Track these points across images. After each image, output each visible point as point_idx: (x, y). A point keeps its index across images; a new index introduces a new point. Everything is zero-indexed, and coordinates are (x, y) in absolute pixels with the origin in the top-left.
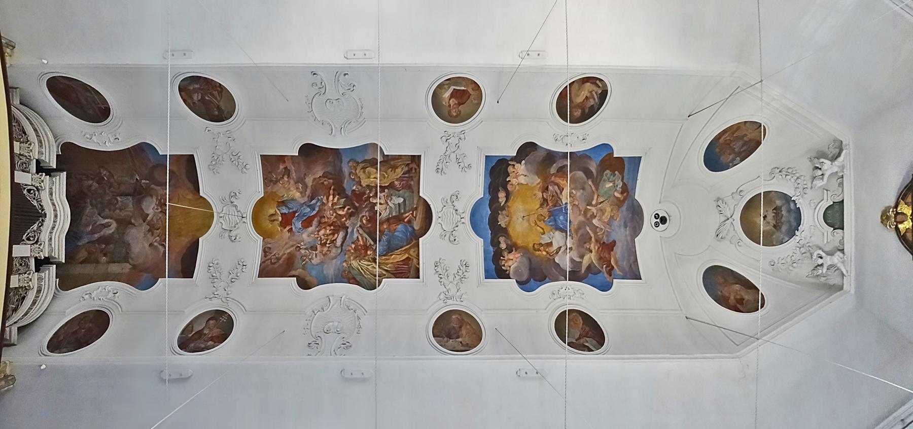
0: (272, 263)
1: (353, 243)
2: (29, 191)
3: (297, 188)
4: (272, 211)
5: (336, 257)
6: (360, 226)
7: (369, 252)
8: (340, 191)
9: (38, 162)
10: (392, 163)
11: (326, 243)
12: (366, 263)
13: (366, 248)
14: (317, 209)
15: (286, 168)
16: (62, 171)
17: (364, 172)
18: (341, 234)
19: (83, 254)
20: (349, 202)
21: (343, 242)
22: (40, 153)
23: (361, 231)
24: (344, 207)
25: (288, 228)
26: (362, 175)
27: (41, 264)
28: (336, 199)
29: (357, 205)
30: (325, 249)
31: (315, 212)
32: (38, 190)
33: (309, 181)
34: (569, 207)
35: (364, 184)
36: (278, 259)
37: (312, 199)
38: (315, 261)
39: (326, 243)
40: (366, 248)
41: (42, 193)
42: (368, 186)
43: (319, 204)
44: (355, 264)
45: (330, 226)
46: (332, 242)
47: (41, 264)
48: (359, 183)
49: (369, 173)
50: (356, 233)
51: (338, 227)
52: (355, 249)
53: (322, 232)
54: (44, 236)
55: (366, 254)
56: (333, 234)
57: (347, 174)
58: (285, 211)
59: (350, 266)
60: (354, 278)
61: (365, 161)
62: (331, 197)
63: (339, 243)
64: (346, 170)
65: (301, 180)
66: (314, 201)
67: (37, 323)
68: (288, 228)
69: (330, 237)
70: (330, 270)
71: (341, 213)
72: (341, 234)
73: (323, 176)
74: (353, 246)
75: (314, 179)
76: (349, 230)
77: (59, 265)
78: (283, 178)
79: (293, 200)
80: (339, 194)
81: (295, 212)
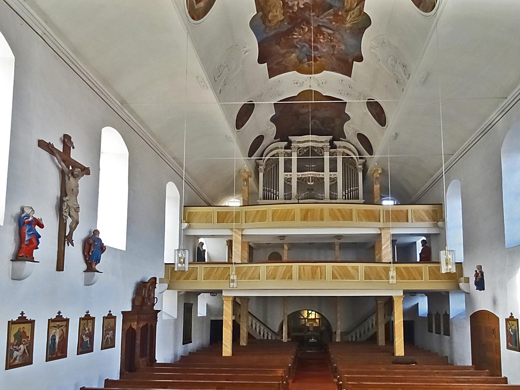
0: (342, 69)
1: (331, 23)
2: (300, 153)
3: (290, 56)
4: (306, 66)
5: (342, 36)
6: (318, 17)
7: (340, 13)
8: (290, 32)
9: (285, 149)
10: (262, 4)
11: (330, 39)
12: (349, 17)
13: (336, 15)
14: (304, 44)
15: (276, 65)
16: (288, 138)
17: (272, 20)
18: (324, 29)
19: (329, 130)
20: (298, 25)
21: (330, 29)
22: (281, 148)
23: (322, 16)
24: (302, 28)
25: (318, 58)
26: (274, 22)
27: (333, 146)
28: (296, 34)
29: (299, 20)
30: (335, 40)
31: (306, 45)
32: (299, 148)
33: (283, 51)
35: (283, 17)
36: (339, 65)
37: (297, 47)
38: (343, 47)
39: (330, 39)
40: (336, 15)
41: (300, 146)
42: (283, 15)
43: (300, 43)
44: (348, 25)
45: (317, 36)
46: (329, 35)
47: (333, 146)
48: (282, 21)
49: (273, 17)
50: (325, 18)
51: (318, 30)
52: (336, 22)
53: (321, 40)
54: (320, 145)
55: (342, 16)
56: (323, 34)
57: (276, 31)
58: (306, 60)
59: (350, 28)
60: (360, 29)
61: (264, 23)
62: (295, 37)
63: (330, 32)
64: (273, 33)
65: (284, 56)
66: (298, 46)
67: (359, 149)
68: (318, 58)
69: (326, 36)
70: (351, 41)
71: (307, 29)
72: (324, 29)
73: (279, 45)
74: (334, 23)
75: (282, 49)
76: (321, 24)
77: (334, 139)
78: (281, 40)
79: (297, 57)
80: (292, 32)
81: (307, 55)
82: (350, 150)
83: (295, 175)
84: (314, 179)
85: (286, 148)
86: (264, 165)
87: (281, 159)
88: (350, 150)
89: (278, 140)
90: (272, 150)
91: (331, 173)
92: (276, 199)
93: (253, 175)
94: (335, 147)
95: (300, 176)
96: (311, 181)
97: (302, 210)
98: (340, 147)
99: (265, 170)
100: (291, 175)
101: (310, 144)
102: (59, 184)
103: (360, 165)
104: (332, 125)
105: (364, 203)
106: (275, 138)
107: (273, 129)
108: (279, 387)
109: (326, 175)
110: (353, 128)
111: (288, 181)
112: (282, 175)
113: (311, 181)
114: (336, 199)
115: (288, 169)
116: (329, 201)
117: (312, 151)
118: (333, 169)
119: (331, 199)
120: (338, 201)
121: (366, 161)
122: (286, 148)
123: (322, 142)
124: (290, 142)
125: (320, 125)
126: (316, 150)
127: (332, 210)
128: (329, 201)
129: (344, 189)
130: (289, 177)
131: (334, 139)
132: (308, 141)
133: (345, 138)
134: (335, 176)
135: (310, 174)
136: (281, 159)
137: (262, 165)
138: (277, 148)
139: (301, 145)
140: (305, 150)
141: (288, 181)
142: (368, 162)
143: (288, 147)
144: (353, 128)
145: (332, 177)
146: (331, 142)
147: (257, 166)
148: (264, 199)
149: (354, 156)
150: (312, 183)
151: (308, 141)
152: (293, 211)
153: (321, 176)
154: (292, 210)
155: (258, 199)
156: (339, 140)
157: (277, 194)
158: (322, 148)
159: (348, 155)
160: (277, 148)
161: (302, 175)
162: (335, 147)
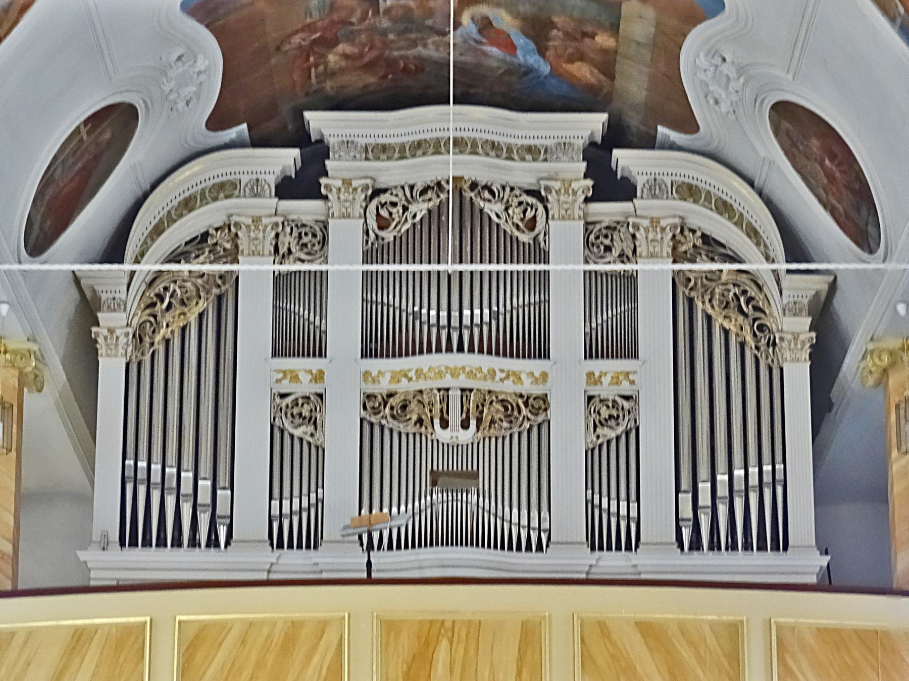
2: (383, 224)
19: (583, 71)
27: (609, 185)
32: (377, 192)
47: (609, 185)
54: (523, 173)
77: (617, 135)
82: (724, 208)
83: (345, 374)
84: (477, 408)
85: (287, 189)
86: (134, 303)
87: (256, 272)
88: (724, 208)
89: (232, 134)
90: (188, 205)
91: (598, 366)
92: (213, 542)
93: (56, 374)
94: (624, 190)
95: (384, 386)
96: (455, 417)
97: (390, 628)
98: (656, 189)
99: (139, 338)
100: (319, 377)
101: (449, 166)
102: (862, 585)
103: (793, 310)
104: (603, 40)
105: (827, 584)
106: (217, 122)
107: (201, 64)
108: (735, 657)
109: (565, 376)
110: (741, 70)
111: (300, 412)
112: (259, 372)
113: (455, 417)
114: (631, 545)
115: (298, 339)
116: (583, 560)
117: (461, 216)
118: (613, 341)
119: (597, 540)
120: (641, 562)
121: (833, 287)
122: (287, 189)
123: (532, 152)
124: (316, 154)
125: (520, 40)
126: (492, 209)
127: (603, 628)
128: (583, 560)
129: (686, 478)
130: (306, 387)
131: (617, 135)
132: (438, 147)
133: (688, 124)
134: (625, 388)
135: (454, 374)
136: (256, 272)
137: (119, 306)
138: (225, 189)
139: (393, 173)
140: (420, 209)
141: (300, 412)
142: (845, 306)
143: (302, 184)
144: (741, 70)
145: (606, 390)
146: (597, 157)
147: (88, 308)
148: (129, 537)
149: (757, 265)
150: (466, 436)
151: (438, 147)
152: (330, 637)
153: (528, 387)
154: (323, 626)
155: (85, 542)
156: (649, 142)
157: (222, 508)
158: (535, 193)
159: (711, 246)
160: (225, 189)
161: (396, 377)
162: (624, 190)
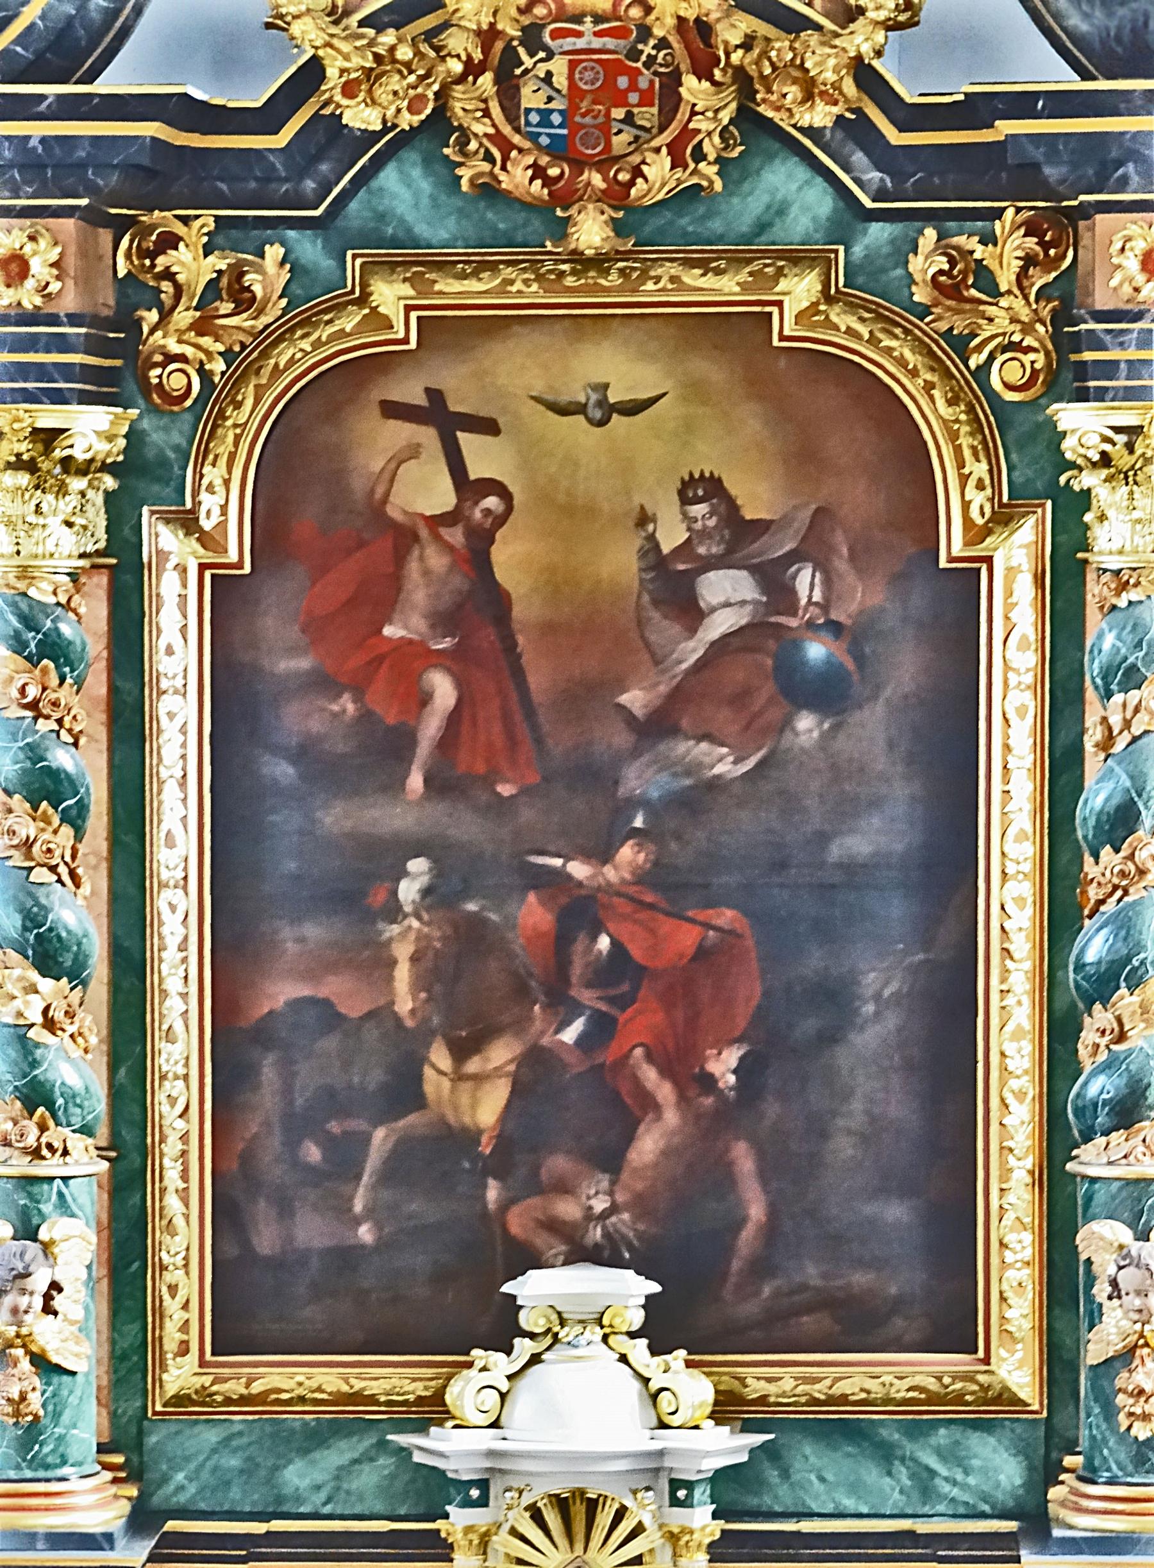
34: (742, 1023)
